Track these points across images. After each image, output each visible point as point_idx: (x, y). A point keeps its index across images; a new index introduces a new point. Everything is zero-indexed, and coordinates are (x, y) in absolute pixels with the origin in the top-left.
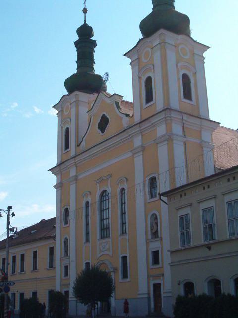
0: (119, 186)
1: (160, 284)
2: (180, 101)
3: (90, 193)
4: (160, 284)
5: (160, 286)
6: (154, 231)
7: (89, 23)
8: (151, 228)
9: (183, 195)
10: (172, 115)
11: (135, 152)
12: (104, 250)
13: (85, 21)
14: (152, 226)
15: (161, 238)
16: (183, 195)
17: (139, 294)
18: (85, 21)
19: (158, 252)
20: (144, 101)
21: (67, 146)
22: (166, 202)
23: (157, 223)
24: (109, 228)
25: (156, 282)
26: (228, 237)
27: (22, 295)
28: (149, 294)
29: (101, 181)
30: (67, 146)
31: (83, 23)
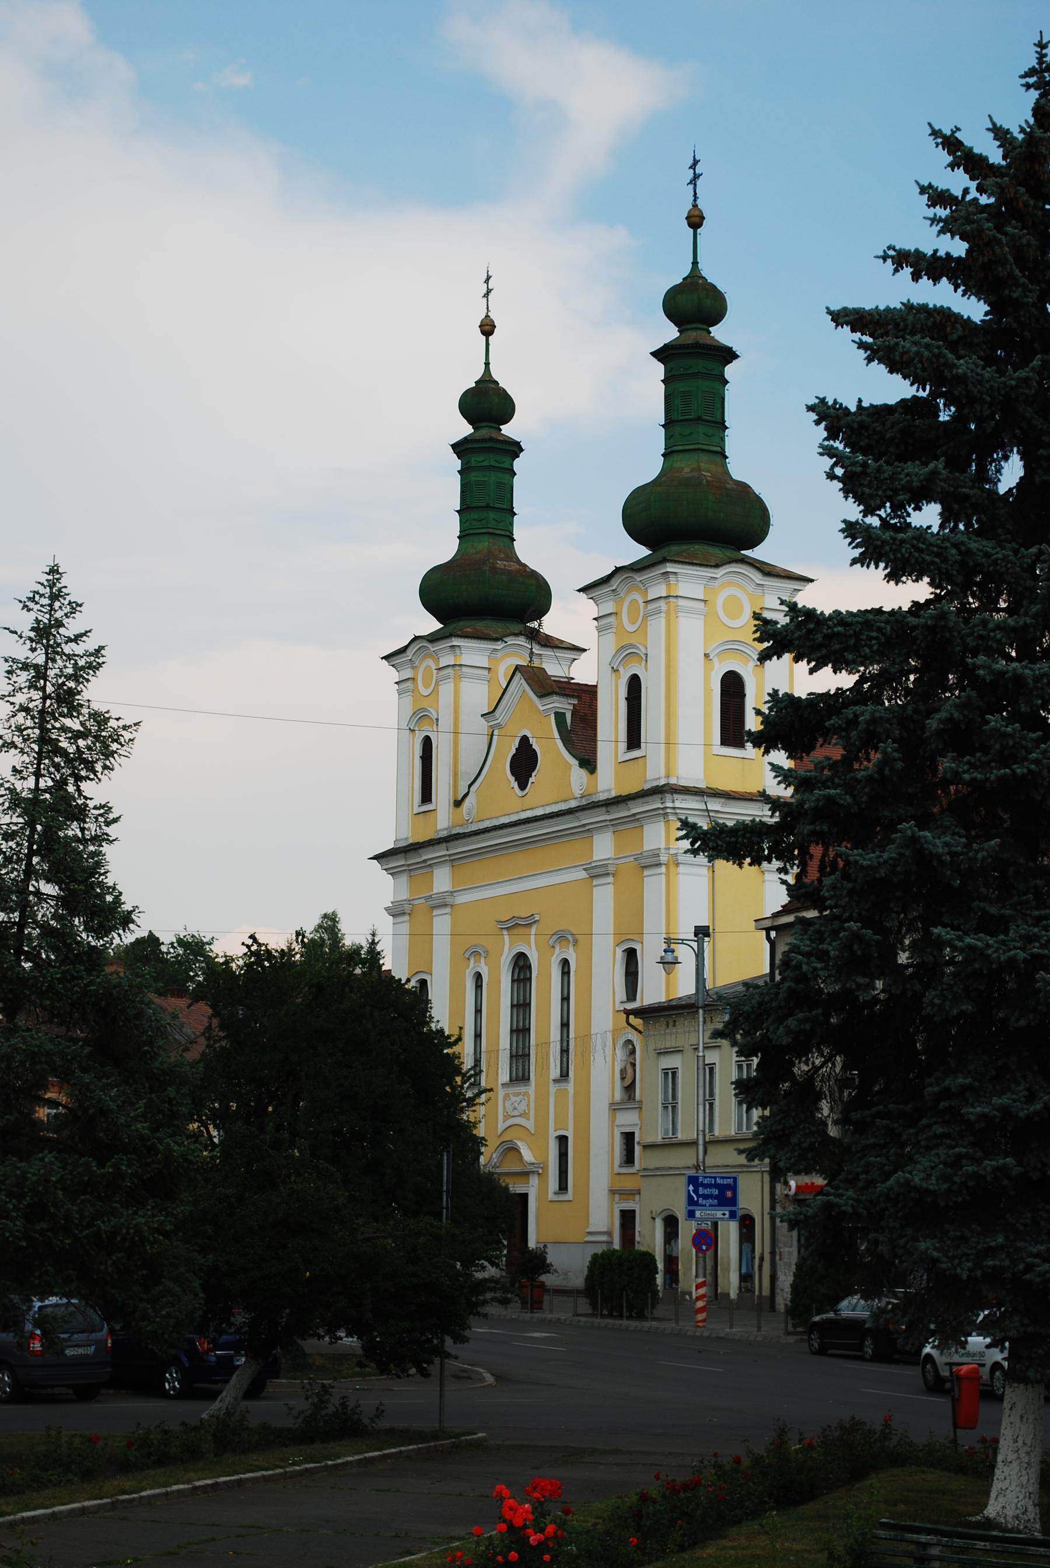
0: (557, 950)
1: (634, 1211)
2: (709, 757)
3: (487, 952)
4: (634, 1211)
5: (634, 1217)
6: (628, 1082)
7: (710, 273)
8: (621, 1074)
9: (671, 1024)
10: (677, 804)
11: (597, 872)
12: (516, 1113)
13: (695, 263)
14: (623, 1071)
15: (641, 1102)
16: (671, 1024)
17: (590, 1233)
18: (695, 263)
19: (633, 1133)
20: (623, 746)
21: (426, 796)
22: (641, 1028)
23: (634, 1065)
24: (529, 1055)
25: (628, 1206)
26: (733, 1133)
27: (850, 544)
28: (609, 1233)
29: (516, 925)
30: (426, 796)
31: (686, 270)
